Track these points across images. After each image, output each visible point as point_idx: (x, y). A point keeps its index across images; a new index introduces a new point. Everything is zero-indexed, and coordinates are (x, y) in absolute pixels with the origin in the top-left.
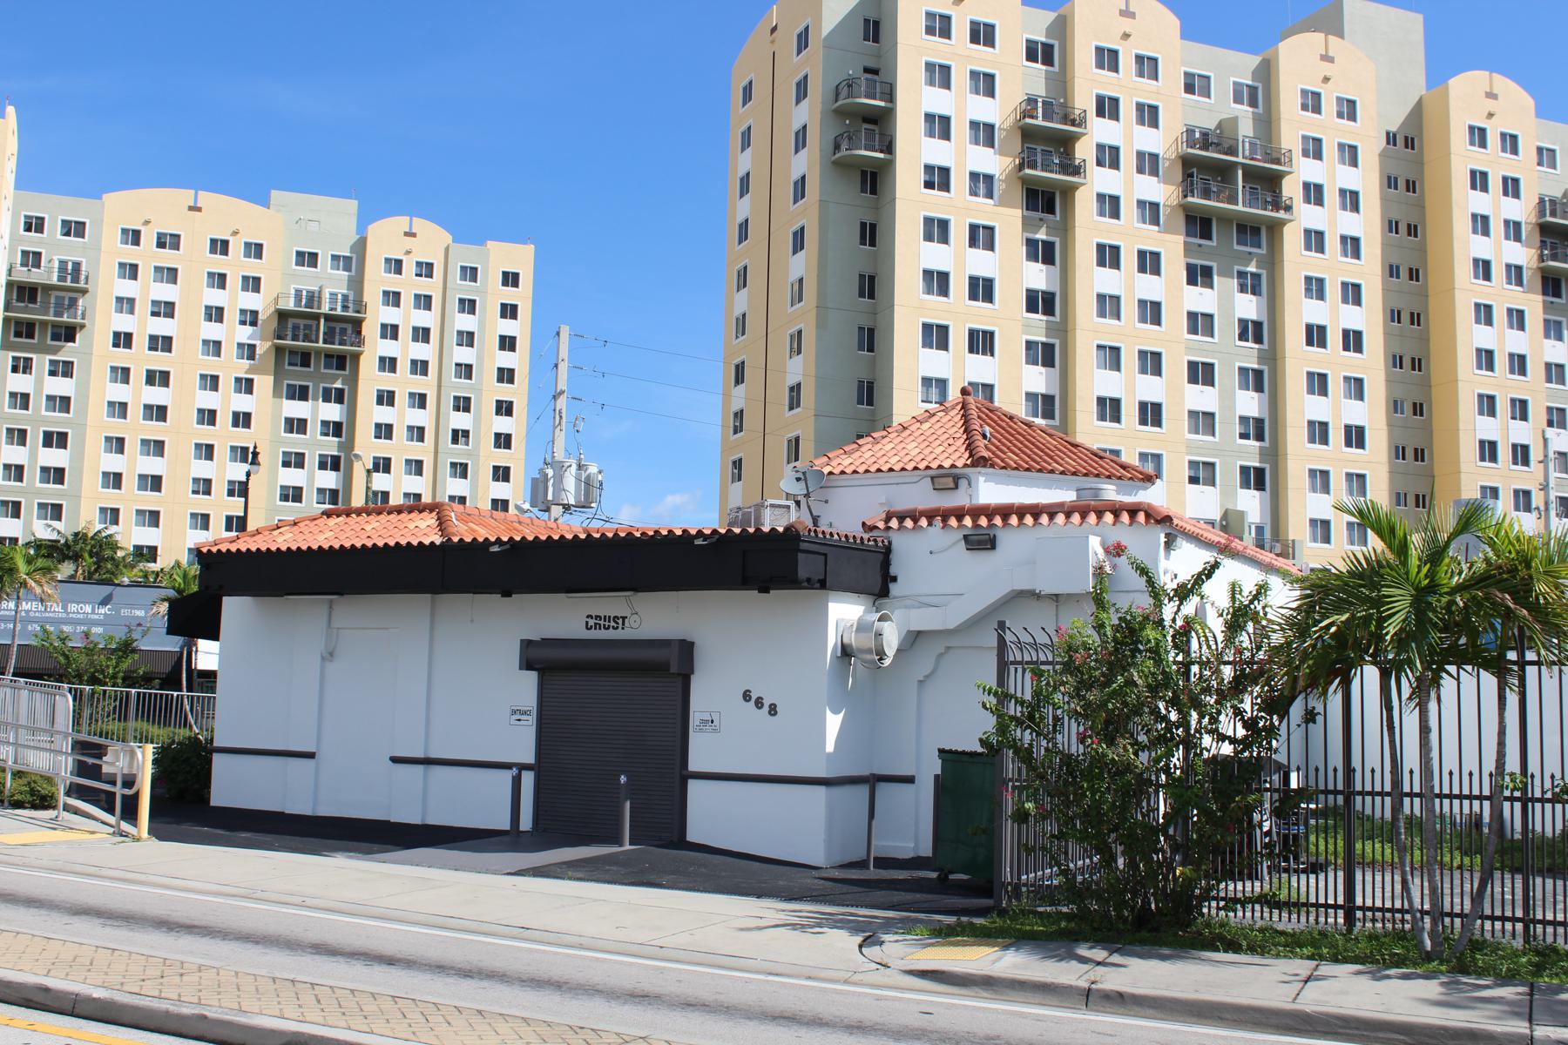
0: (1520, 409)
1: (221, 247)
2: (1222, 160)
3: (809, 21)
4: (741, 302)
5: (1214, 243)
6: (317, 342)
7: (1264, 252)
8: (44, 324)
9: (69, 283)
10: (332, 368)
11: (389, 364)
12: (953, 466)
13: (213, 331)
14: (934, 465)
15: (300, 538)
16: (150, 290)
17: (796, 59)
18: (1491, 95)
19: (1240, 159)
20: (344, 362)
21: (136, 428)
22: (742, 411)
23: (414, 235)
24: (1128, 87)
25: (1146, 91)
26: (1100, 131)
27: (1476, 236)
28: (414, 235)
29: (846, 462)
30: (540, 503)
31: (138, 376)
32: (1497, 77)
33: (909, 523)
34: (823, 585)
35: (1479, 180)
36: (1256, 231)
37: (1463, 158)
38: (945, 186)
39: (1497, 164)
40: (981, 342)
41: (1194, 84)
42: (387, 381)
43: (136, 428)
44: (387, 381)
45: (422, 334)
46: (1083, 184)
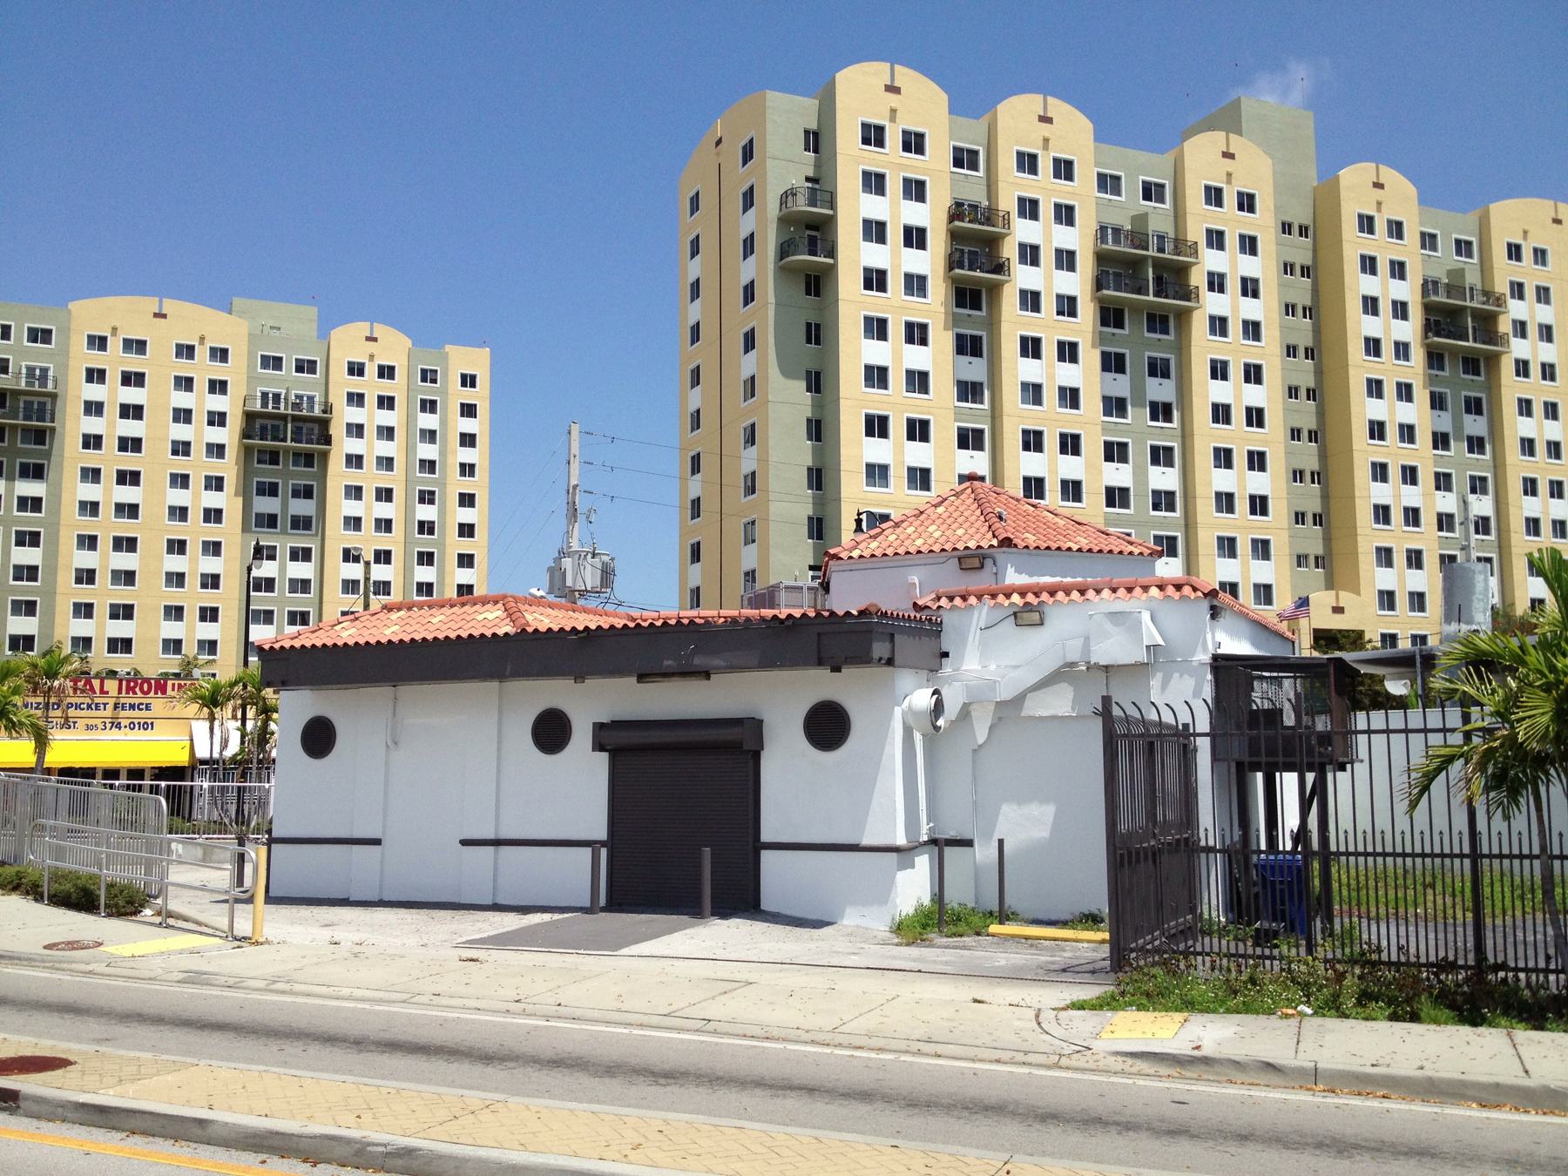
0: (1410, 475)
1: (186, 351)
2: (1453, 304)
3: (752, 134)
4: (695, 398)
5: (1126, 332)
6: (284, 440)
7: (1173, 338)
8: (14, 427)
9: (37, 388)
10: (30, 443)
11: (355, 461)
12: (979, 547)
13: (181, 432)
14: (960, 546)
15: (366, 632)
16: (114, 394)
17: (741, 170)
18: (1378, 185)
19: (1150, 253)
20: (314, 460)
21: (108, 526)
22: (699, 499)
23: (375, 340)
24: (1046, 188)
25: (1063, 191)
26: (1212, 260)
27: (1061, 272)
28: (375, 340)
29: (874, 545)
30: (556, 590)
31: (109, 476)
32: (1383, 169)
33: (958, 601)
34: (890, 662)
35: (1369, 264)
36: (1164, 320)
37: (1354, 244)
38: (882, 287)
39: (1383, 248)
40: (918, 430)
41: (1108, 183)
42: (354, 477)
43: (108, 526)
44: (354, 477)
45: (387, 433)
46: (1007, 281)
